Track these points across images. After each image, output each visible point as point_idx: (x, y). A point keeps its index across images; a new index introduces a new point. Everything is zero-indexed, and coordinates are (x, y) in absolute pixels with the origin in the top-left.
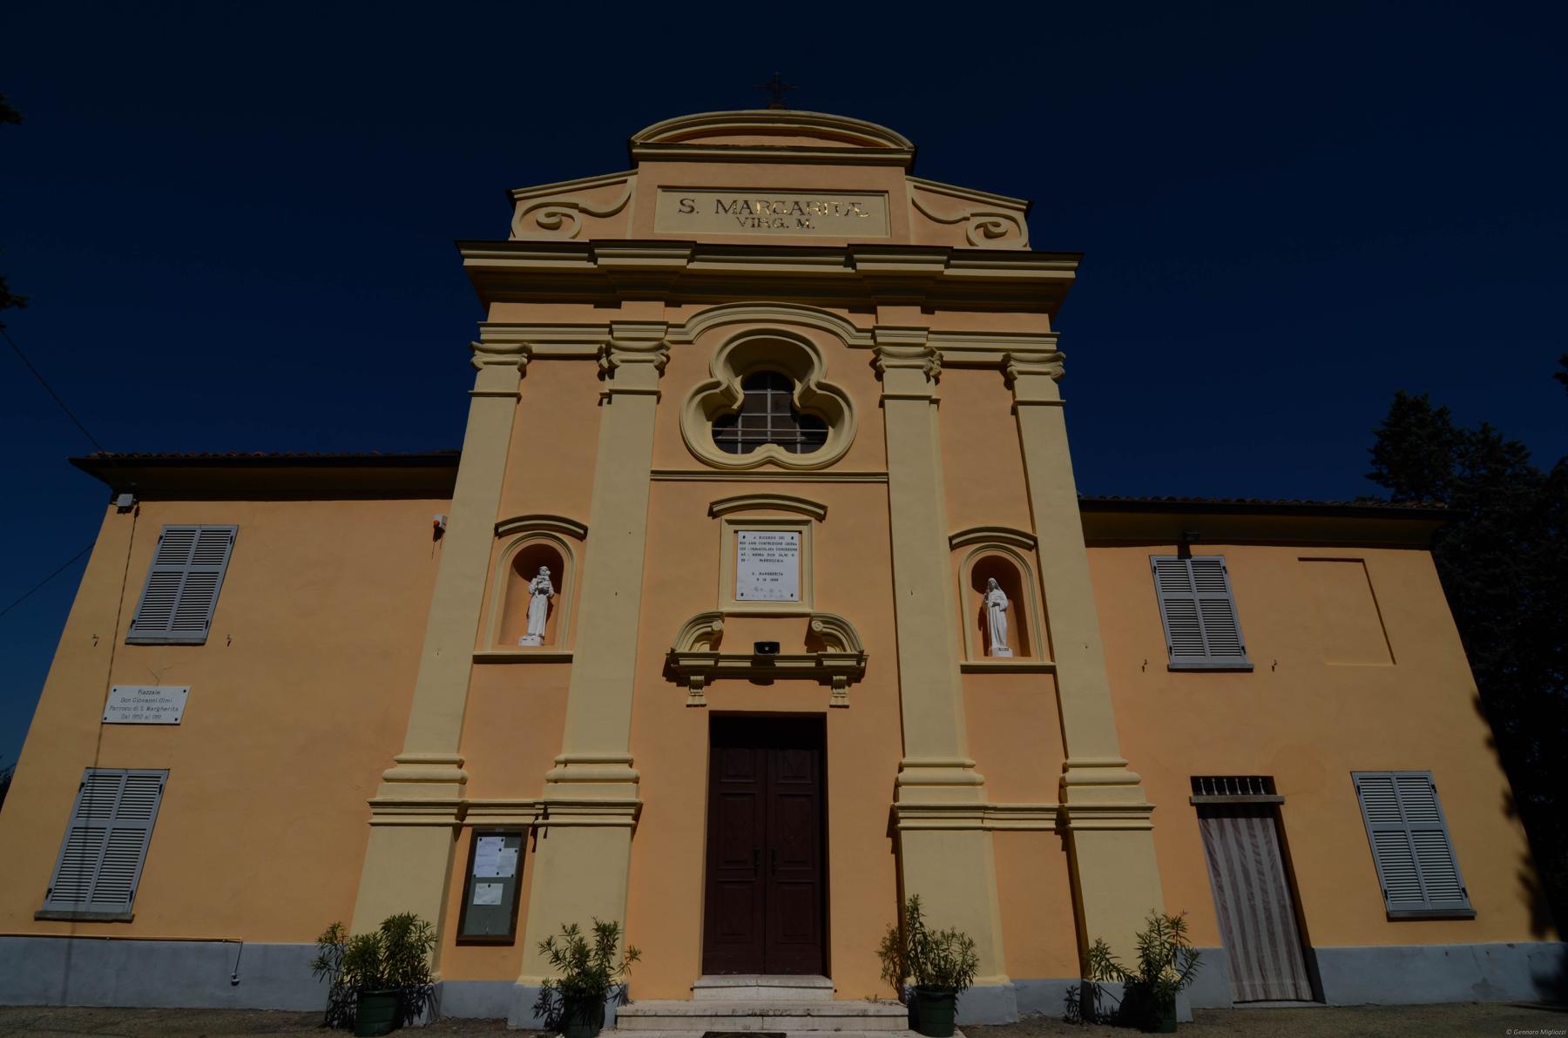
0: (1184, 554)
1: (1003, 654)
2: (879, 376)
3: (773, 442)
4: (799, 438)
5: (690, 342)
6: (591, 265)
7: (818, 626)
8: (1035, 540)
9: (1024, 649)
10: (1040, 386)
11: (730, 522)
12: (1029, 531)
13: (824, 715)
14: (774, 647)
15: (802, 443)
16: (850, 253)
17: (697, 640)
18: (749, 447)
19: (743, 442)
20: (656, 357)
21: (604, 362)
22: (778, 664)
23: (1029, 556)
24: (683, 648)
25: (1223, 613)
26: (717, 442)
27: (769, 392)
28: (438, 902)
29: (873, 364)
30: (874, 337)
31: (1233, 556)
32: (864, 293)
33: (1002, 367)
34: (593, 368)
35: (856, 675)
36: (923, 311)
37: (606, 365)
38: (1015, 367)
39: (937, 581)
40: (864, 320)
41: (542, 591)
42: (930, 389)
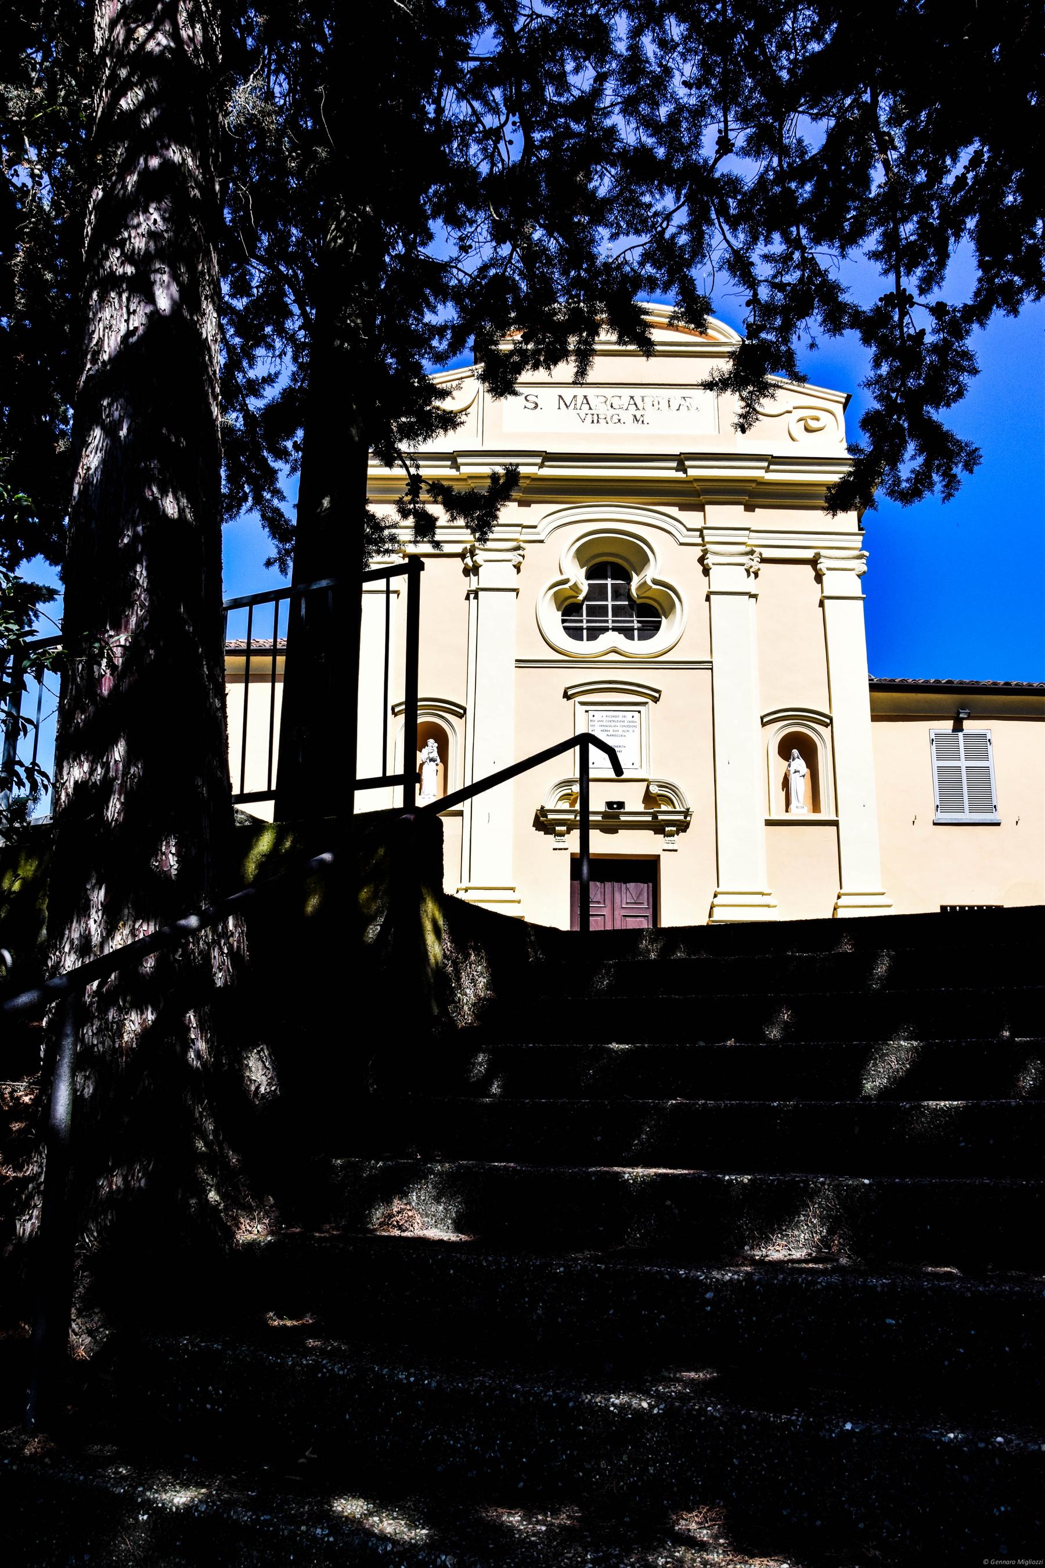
0: (958, 728)
1: (801, 810)
2: (706, 572)
3: (614, 629)
4: (636, 625)
5: (542, 541)
6: (453, 472)
7: (654, 789)
8: (831, 719)
9: (816, 806)
10: (846, 580)
11: (582, 703)
12: (827, 712)
13: (657, 858)
14: (621, 805)
15: (639, 629)
16: (681, 460)
17: (560, 799)
18: (594, 633)
19: (588, 629)
20: (514, 556)
21: (468, 560)
22: (623, 818)
23: (825, 732)
24: (548, 806)
25: (982, 780)
26: (565, 628)
27: (609, 582)
28: (987, 680)
29: (701, 560)
30: (702, 536)
31: (998, 731)
32: (694, 496)
33: (813, 562)
34: (458, 564)
35: (683, 827)
36: (746, 510)
37: (471, 564)
38: (822, 566)
39: (752, 753)
40: (694, 519)
41: (432, 760)
42: (750, 585)
